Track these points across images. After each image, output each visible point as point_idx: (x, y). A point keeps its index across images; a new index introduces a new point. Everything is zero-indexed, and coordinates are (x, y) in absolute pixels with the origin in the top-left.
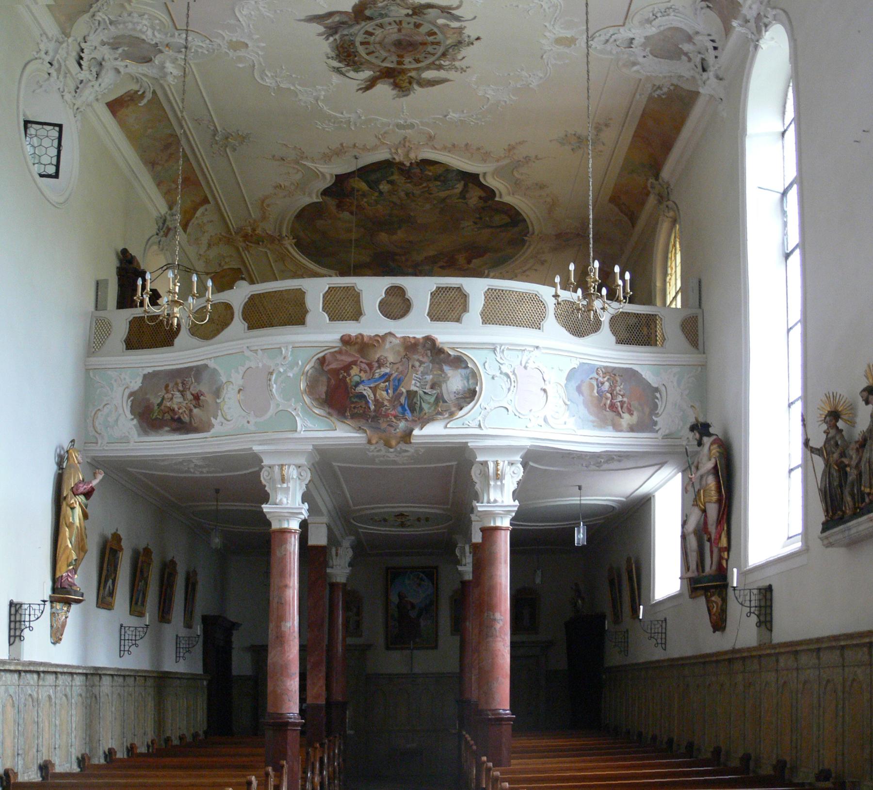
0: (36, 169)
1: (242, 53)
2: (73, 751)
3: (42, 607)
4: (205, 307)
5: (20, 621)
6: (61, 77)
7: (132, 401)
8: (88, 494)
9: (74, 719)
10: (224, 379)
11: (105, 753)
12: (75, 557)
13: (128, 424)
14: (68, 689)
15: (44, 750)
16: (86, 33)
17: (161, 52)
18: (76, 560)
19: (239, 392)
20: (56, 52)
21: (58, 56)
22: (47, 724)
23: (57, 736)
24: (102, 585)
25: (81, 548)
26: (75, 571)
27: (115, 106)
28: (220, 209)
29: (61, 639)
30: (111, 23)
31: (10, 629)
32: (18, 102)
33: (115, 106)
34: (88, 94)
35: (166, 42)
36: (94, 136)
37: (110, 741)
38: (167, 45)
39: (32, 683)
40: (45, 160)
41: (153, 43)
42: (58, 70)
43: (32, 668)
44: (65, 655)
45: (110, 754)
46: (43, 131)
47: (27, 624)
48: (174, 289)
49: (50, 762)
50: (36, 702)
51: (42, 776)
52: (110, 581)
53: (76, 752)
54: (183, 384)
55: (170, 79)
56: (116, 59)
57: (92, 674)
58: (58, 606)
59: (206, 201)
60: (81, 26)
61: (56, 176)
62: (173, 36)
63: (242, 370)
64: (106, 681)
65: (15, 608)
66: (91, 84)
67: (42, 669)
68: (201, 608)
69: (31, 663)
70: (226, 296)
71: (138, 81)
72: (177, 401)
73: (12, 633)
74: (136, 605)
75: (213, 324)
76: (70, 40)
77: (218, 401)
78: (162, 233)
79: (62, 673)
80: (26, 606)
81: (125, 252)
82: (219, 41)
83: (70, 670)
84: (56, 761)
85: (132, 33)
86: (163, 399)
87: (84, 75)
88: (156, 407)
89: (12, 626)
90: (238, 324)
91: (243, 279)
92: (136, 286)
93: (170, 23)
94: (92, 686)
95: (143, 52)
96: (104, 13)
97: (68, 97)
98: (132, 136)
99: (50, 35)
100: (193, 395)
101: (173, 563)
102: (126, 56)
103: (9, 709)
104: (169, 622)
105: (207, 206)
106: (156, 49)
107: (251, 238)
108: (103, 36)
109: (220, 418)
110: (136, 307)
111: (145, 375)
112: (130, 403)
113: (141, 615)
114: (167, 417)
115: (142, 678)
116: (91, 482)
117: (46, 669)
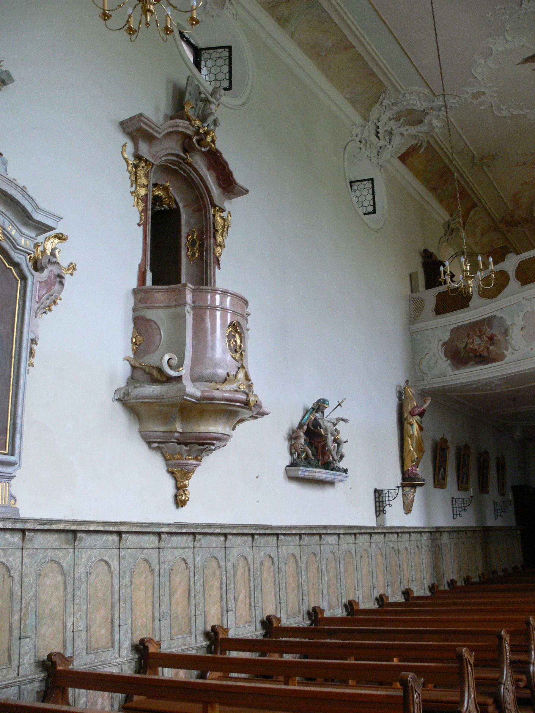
0: (361, 211)
1: (482, 99)
2: (426, 582)
3: (397, 491)
4: (490, 275)
5: (382, 501)
6: (368, 148)
7: (445, 348)
8: (421, 414)
9: (424, 561)
10: (509, 323)
11: (448, 582)
12: (416, 456)
13: (444, 364)
14: (418, 542)
15: (405, 582)
16: (379, 116)
17: (428, 114)
18: (417, 458)
19: (522, 329)
20: (362, 133)
21: (364, 136)
22: (406, 565)
23: (414, 573)
24: (437, 472)
25: (420, 450)
26: (417, 465)
27: (403, 158)
28: (486, 209)
29: (411, 511)
30: (393, 105)
31: (376, 507)
32: (344, 171)
33: (403, 158)
34: (386, 155)
35: (430, 107)
36: (391, 176)
37: (451, 575)
38: (431, 108)
39: (393, 540)
40: (366, 203)
41: (422, 109)
42: (365, 145)
43: (393, 531)
44: (414, 520)
45: (452, 583)
46: (362, 185)
47: (387, 503)
48: (467, 268)
49: (410, 589)
50: (398, 552)
51: (405, 598)
52: (442, 470)
53: (427, 582)
54: (480, 331)
55: (437, 130)
56: (400, 127)
57: (435, 532)
58: (408, 489)
59: (475, 205)
60: (374, 113)
61: (374, 212)
62: (434, 101)
63: (521, 314)
64: (445, 536)
65: (378, 494)
66: (388, 147)
67: (399, 531)
68: (510, 480)
69: (392, 527)
70: (501, 266)
71: (416, 138)
72: (477, 343)
73: (378, 509)
74: (462, 484)
75: (495, 287)
76: (370, 123)
77: (507, 338)
78: (448, 233)
79: (414, 532)
80: (386, 491)
81: (425, 251)
82: (465, 95)
83: (419, 530)
84: (414, 589)
85: (410, 107)
86: (467, 343)
87: (382, 143)
88: (462, 350)
89: (377, 504)
90: (514, 283)
91: (511, 252)
92: (440, 272)
93: (431, 94)
94: (436, 539)
95: (415, 118)
96: (387, 100)
97: (374, 160)
98: (418, 174)
99: (357, 124)
100: (487, 337)
101: (486, 453)
102: (406, 123)
103: (379, 556)
104: (487, 492)
105: (476, 209)
106: (425, 113)
107: (511, 223)
108: (389, 114)
109: (510, 350)
110: (442, 285)
111: (452, 331)
112: (443, 350)
113: (466, 490)
114: (471, 355)
115: (471, 532)
116: (422, 406)
117: (402, 531)
